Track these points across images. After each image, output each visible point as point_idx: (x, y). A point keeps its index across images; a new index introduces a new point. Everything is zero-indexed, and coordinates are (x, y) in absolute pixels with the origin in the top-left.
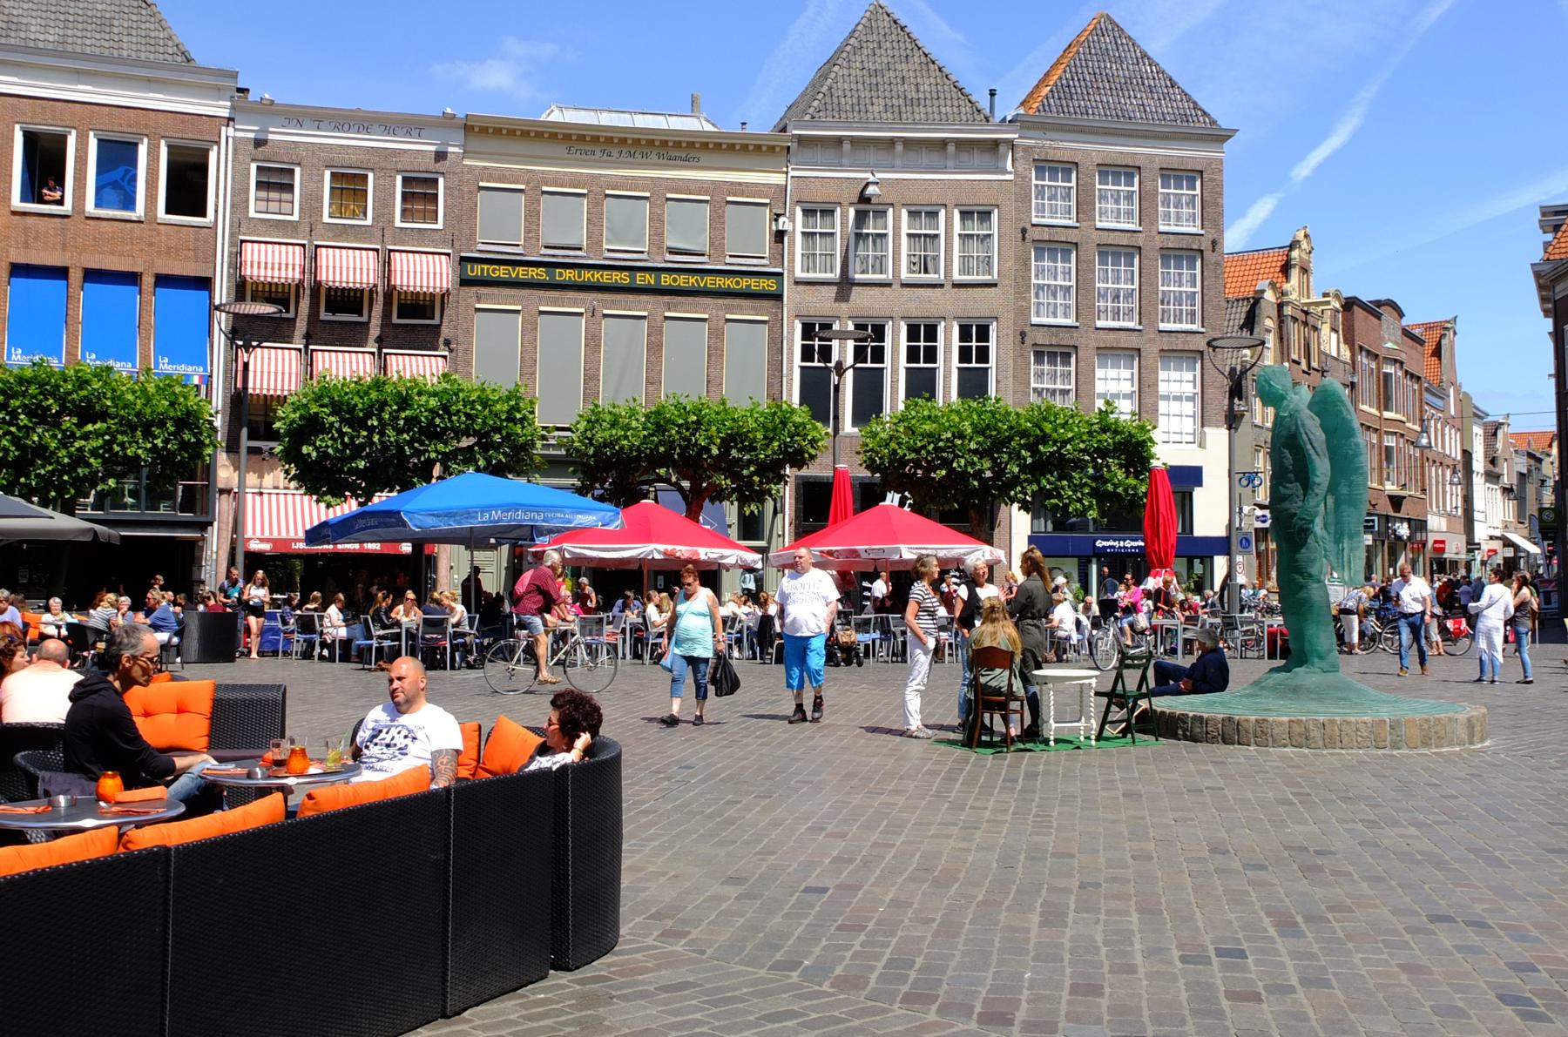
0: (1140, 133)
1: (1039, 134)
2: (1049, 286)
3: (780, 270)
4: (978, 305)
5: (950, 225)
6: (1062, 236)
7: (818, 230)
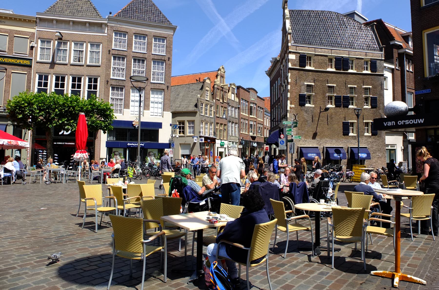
0: (142, 24)
1: (116, 23)
2: (118, 68)
3: (32, 58)
4: (94, 72)
5: (87, 48)
6: (122, 53)
7: (46, 47)
